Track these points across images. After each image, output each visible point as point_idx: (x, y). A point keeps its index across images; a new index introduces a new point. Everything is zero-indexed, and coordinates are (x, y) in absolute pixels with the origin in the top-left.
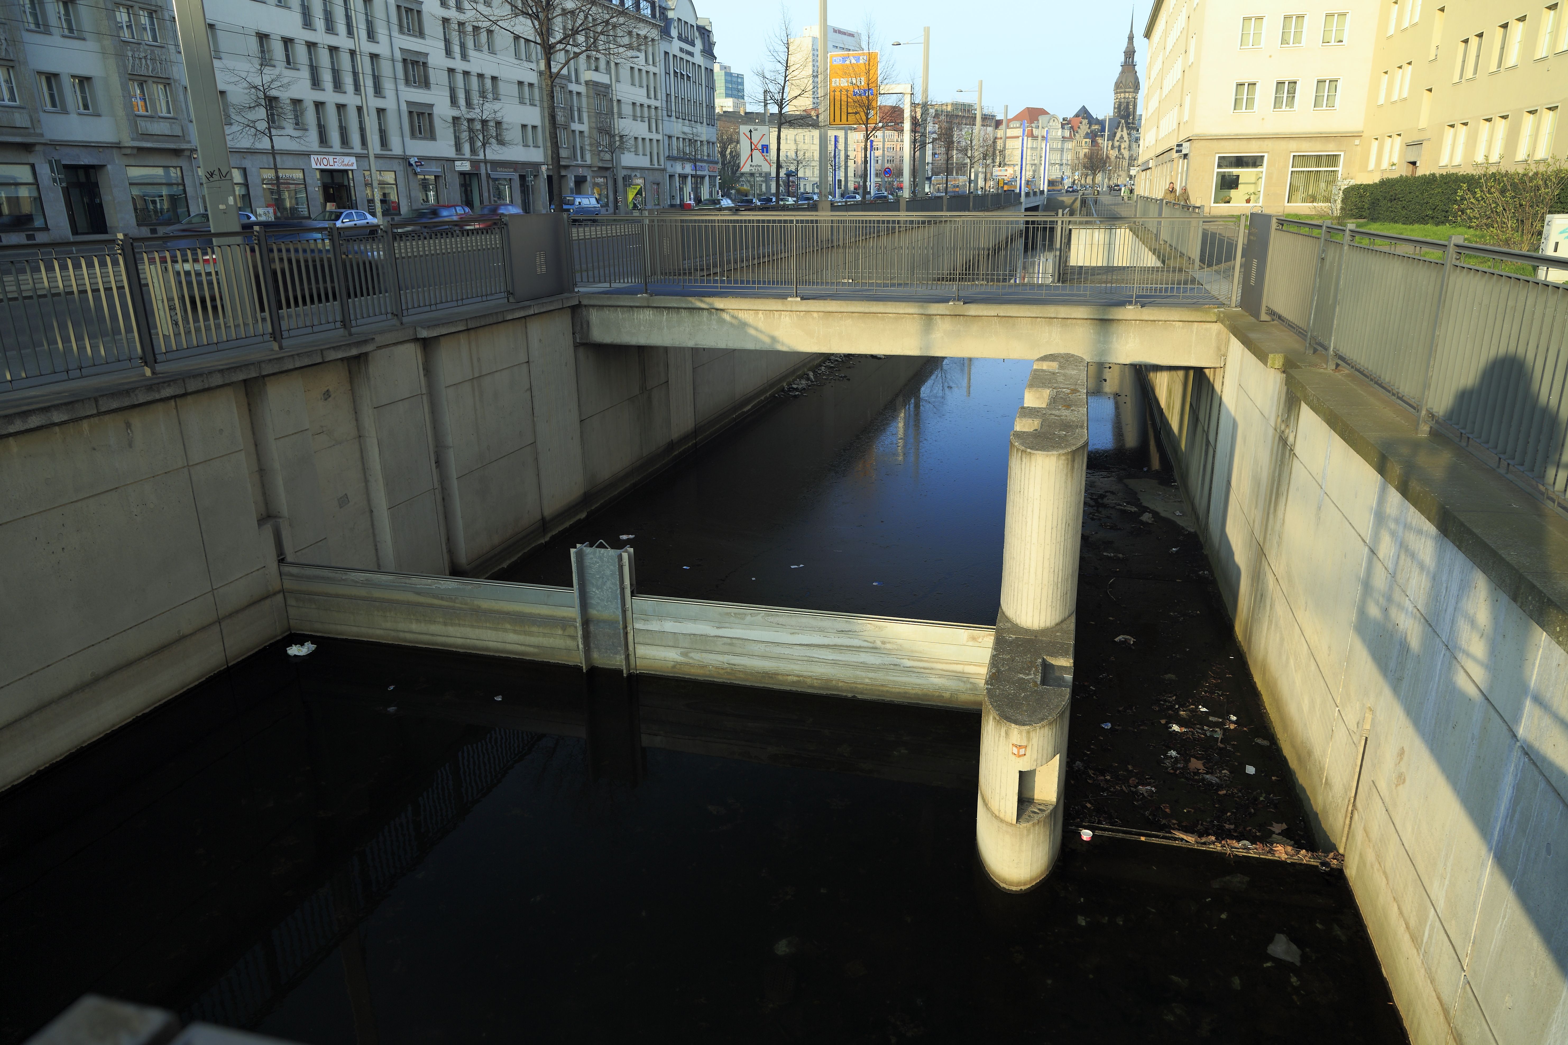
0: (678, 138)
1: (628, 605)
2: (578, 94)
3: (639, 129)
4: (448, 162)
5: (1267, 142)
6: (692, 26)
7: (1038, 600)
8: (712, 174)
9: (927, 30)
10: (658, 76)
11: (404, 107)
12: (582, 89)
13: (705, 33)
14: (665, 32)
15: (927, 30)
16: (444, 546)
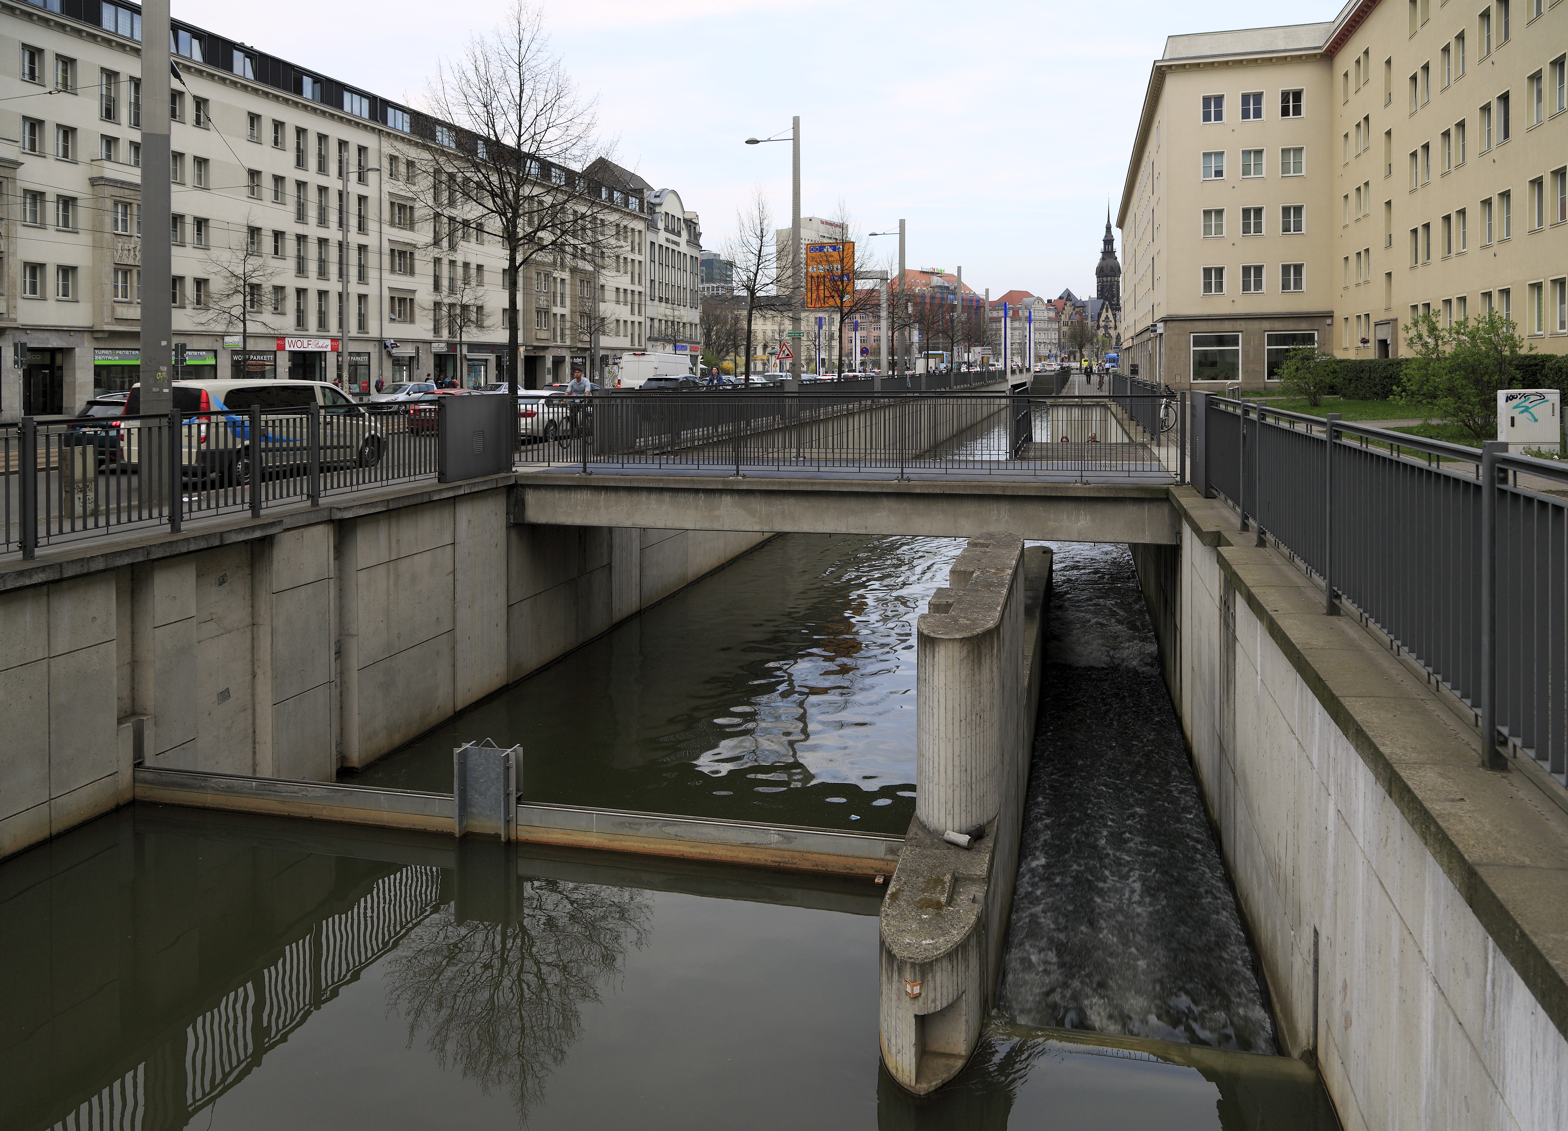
0: (660, 320)
1: (512, 815)
2: (563, 280)
3: (623, 312)
4: (425, 345)
5: (1239, 322)
6: (679, 219)
7: (950, 804)
8: (693, 353)
9: (902, 223)
10: (643, 264)
11: (386, 294)
12: (566, 275)
13: (691, 224)
14: (652, 226)
15: (902, 223)
16: (334, 748)
